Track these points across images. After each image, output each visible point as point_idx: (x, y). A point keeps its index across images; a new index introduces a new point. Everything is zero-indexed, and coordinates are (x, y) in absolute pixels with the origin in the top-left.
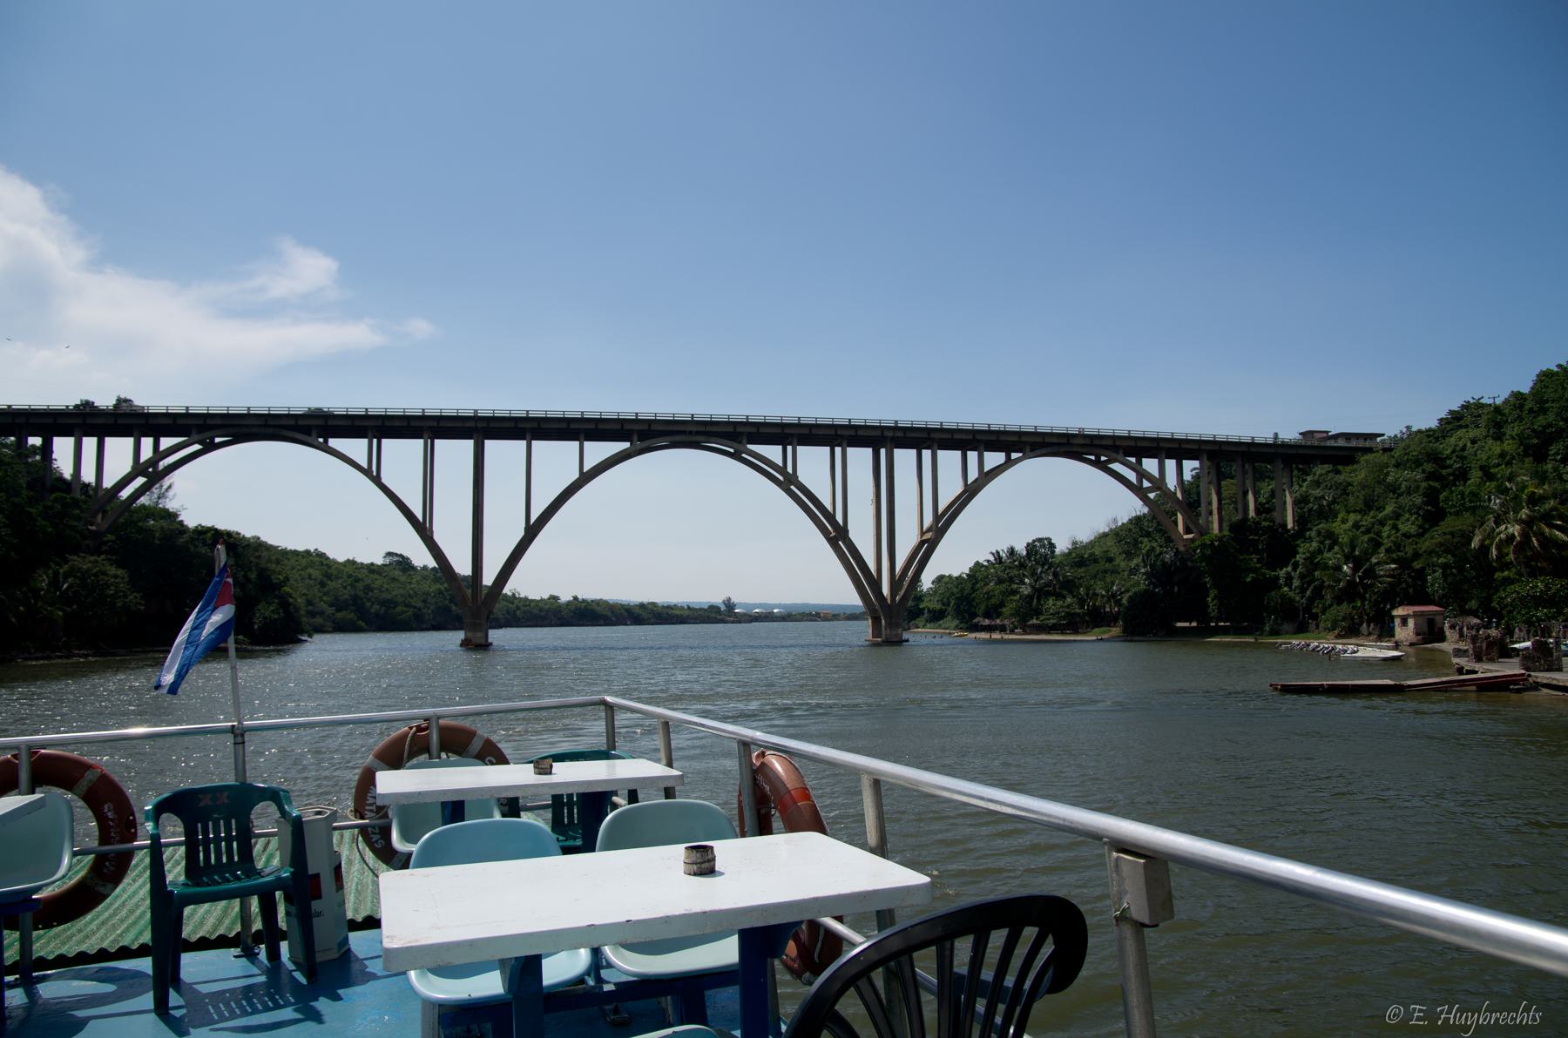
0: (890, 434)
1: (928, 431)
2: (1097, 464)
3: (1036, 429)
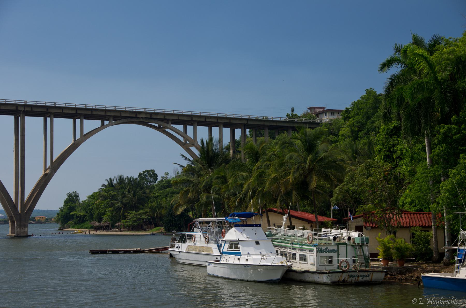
0: (22, 109)
1: (77, 110)
2: (158, 128)
3: (200, 113)
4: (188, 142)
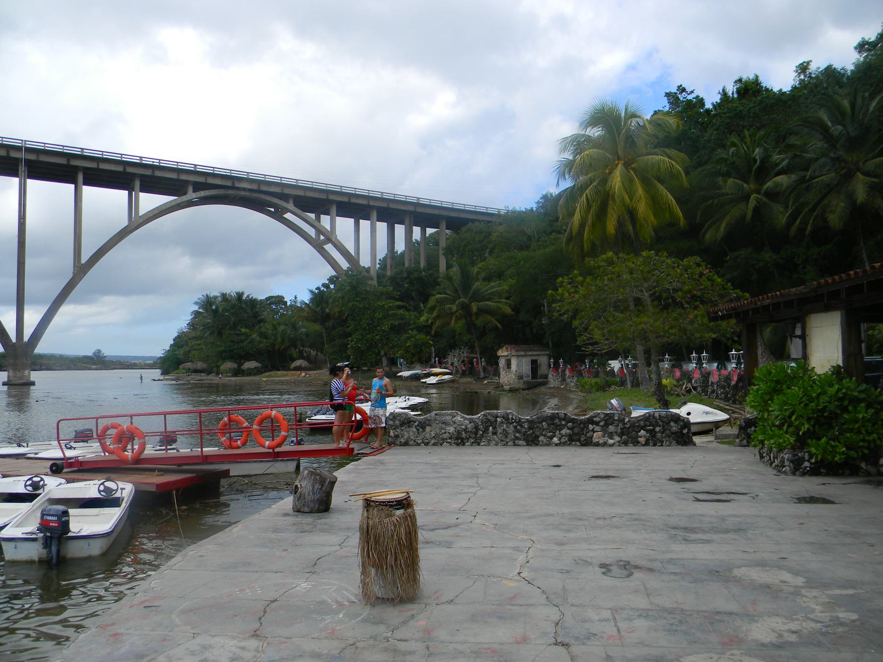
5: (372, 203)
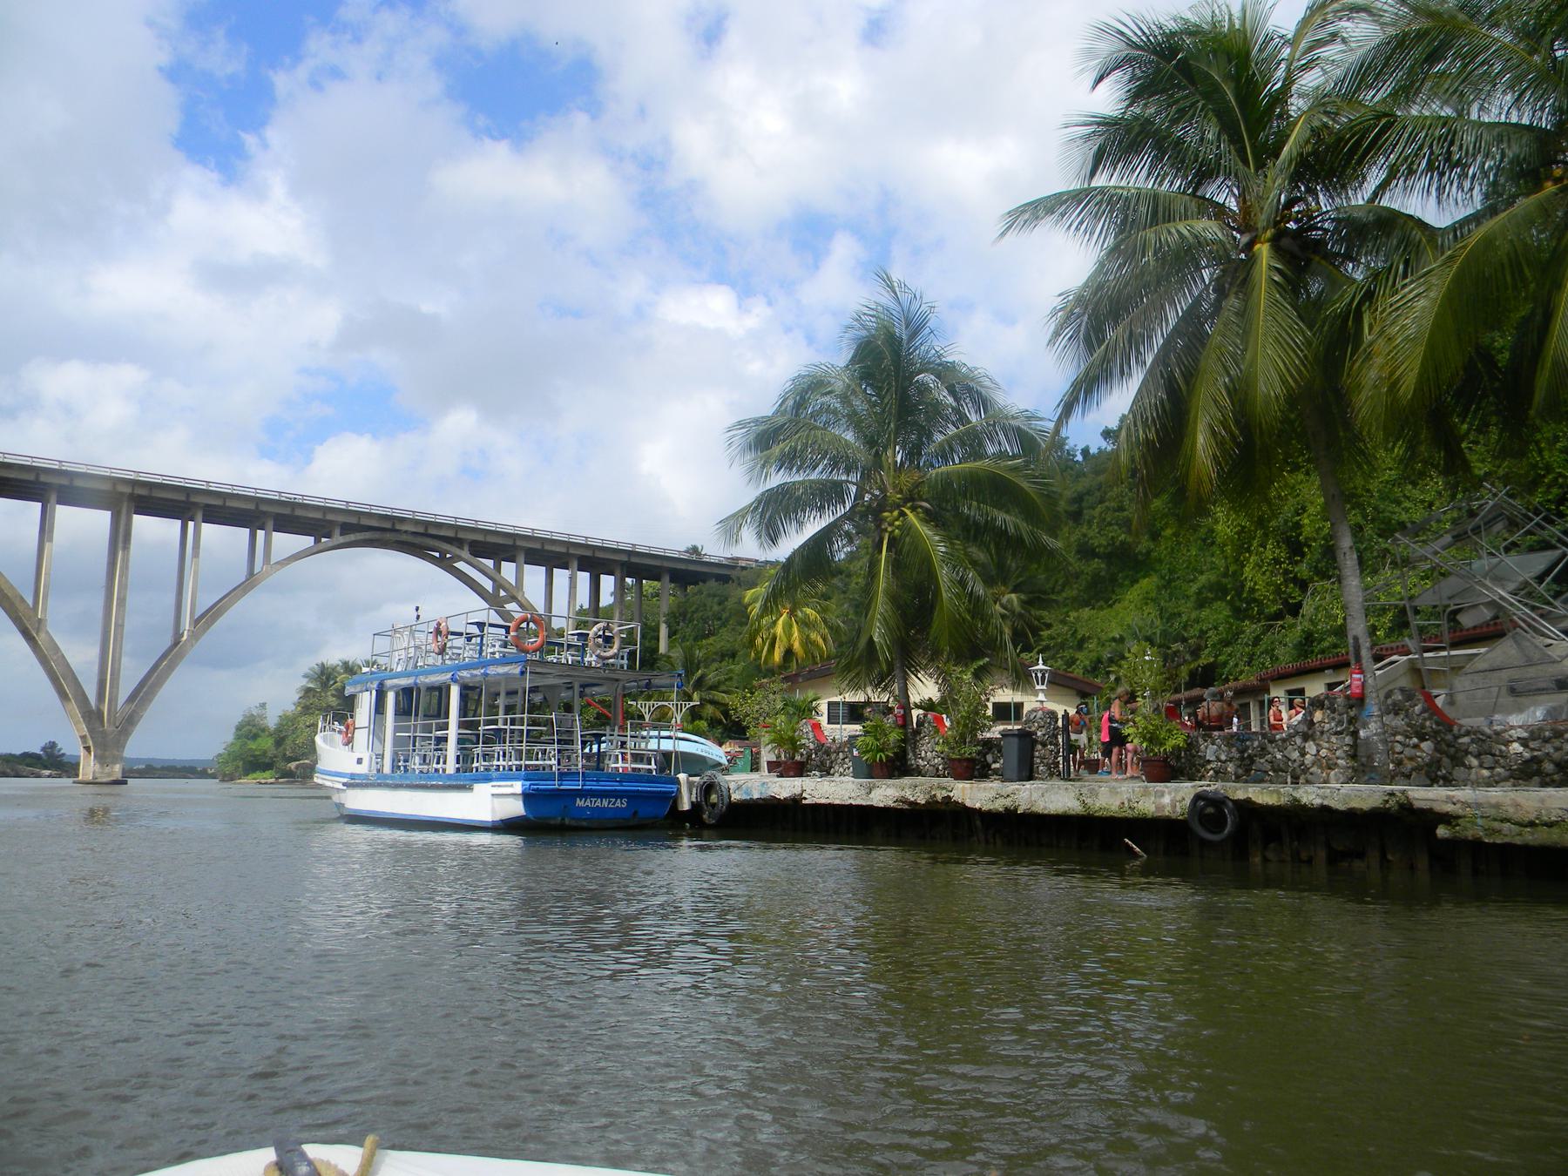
4: (502, 593)
5: (572, 551)
